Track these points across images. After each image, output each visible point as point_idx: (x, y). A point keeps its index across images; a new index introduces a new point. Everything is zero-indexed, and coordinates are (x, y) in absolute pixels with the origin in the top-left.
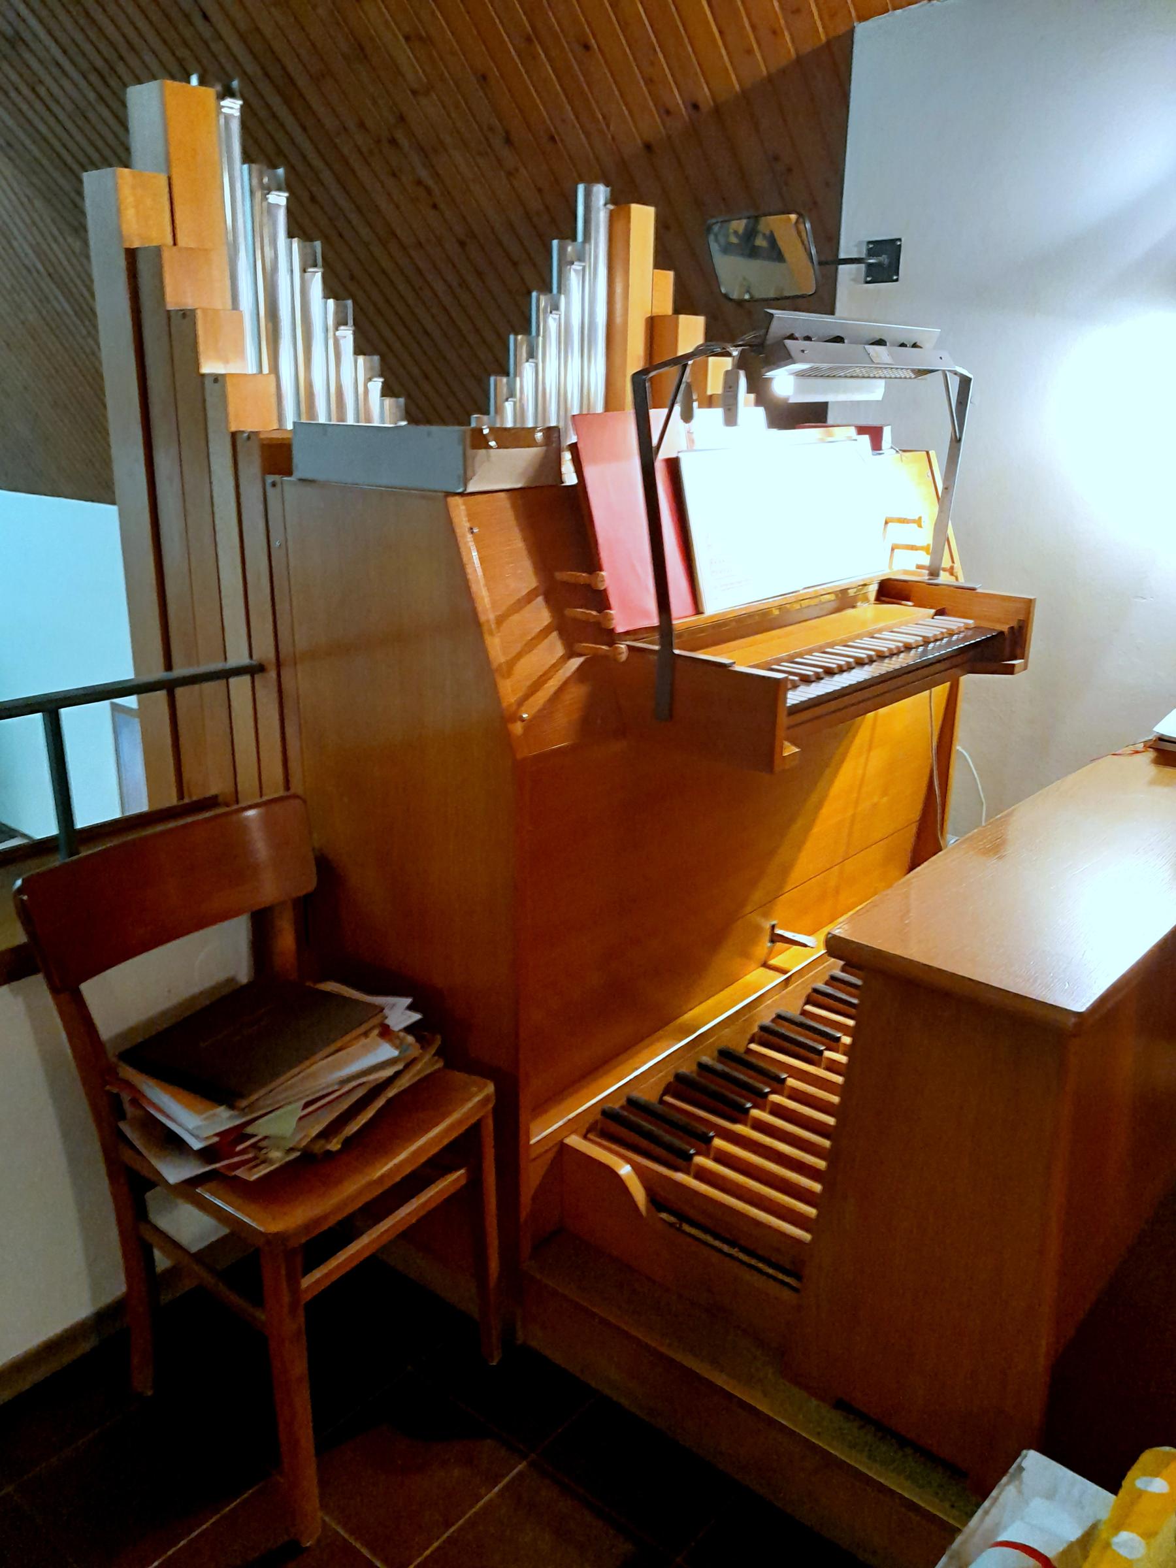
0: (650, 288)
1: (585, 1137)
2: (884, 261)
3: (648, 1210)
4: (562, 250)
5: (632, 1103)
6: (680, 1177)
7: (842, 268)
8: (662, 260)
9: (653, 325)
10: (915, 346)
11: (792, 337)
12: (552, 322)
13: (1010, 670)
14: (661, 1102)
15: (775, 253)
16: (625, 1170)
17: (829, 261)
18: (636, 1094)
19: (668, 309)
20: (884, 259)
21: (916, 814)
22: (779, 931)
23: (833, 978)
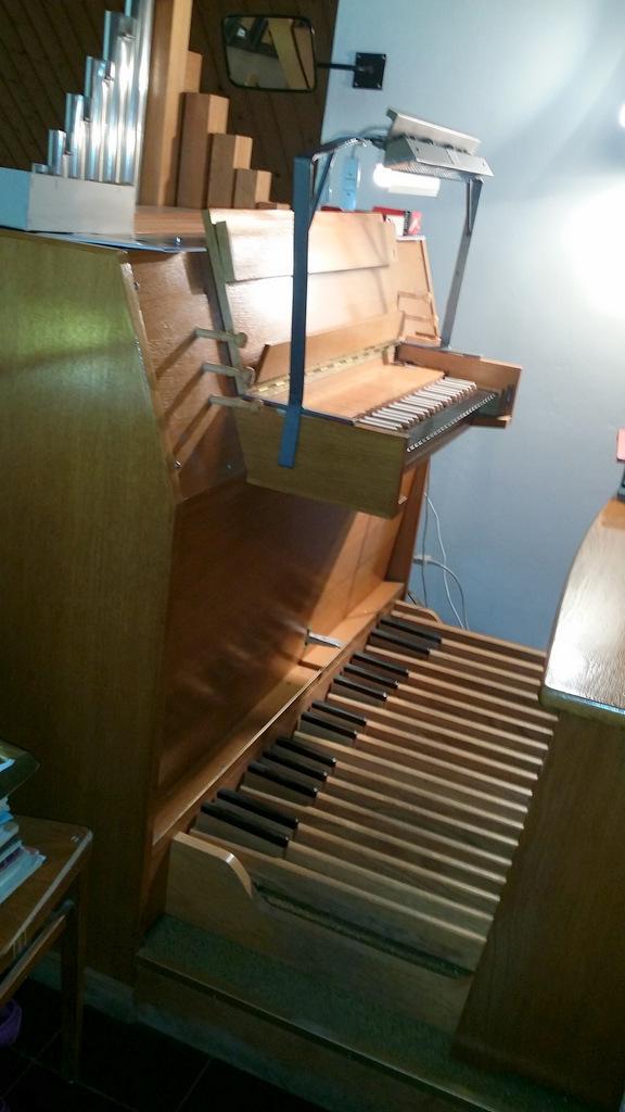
0: (183, 68)
1: (187, 832)
2: (369, 71)
3: (253, 892)
4: (115, 24)
5: (221, 795)
6: (280, 862)
7: (334, 73)
8: (193, 46)
9: (184, 98)
10: (465, 152)
11: (412, 138)
12: (106, 89)
13: (503, 425)
14: (238, 788)
15: (270, 52)
16: (230, 858)
17: (324, 65)
18: (221, 787)
19: (194, 87)
20: (371, 69)
21: (394, 534)
22: (312, 635)
23: (346, 670)
